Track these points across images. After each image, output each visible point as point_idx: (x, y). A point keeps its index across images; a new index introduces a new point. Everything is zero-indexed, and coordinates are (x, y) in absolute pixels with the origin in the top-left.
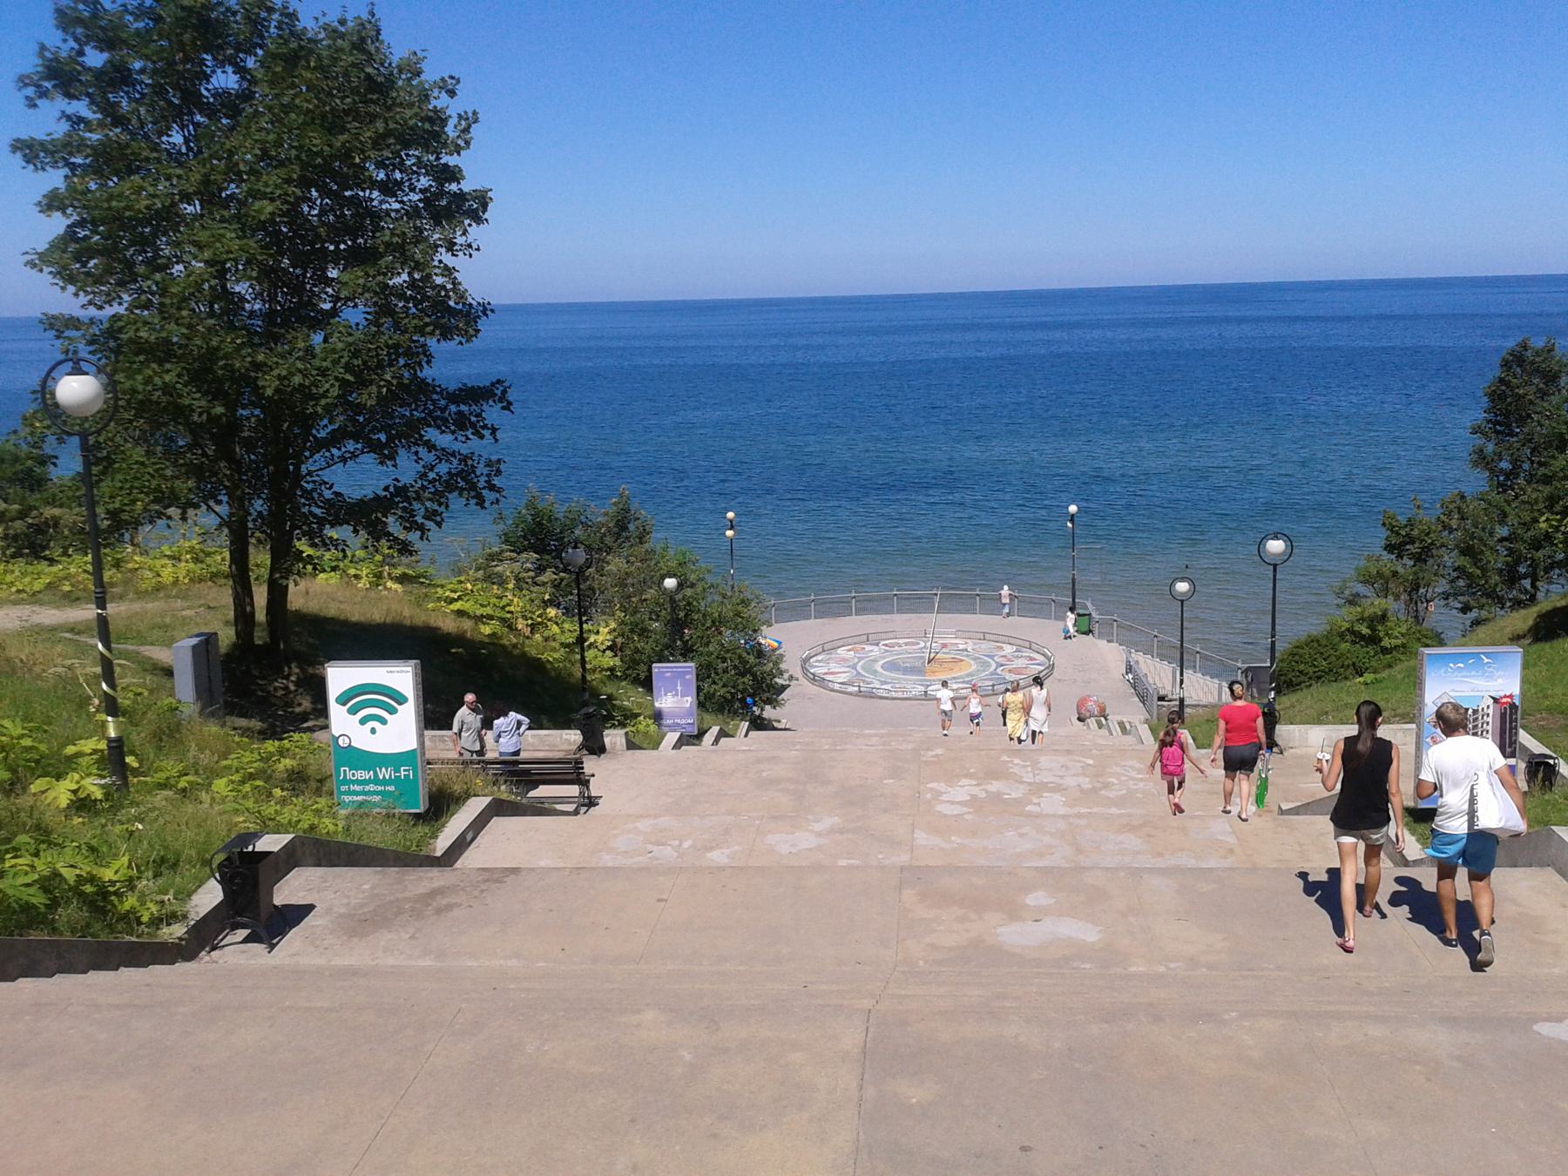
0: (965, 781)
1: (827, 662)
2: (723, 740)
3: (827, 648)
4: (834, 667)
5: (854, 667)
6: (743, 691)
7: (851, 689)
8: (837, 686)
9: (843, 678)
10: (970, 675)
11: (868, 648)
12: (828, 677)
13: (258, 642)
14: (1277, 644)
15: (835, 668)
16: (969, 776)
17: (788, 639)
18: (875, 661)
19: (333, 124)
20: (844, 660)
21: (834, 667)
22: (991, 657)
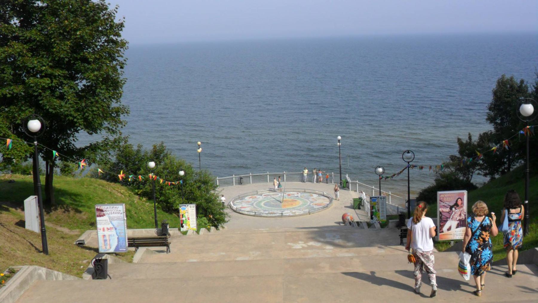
0: (300, 242)
1: (241, 203)
2: (455, 202)
3: (241, 198)
4: (244, 205)
5: (252, 204)
6: (211, 215)
7: (252, 214)
8: (246, 213)
9: (248, 209)
10: (300, 206)
11: (258, 197)
12: (242, 209)
13: (50, 92)
14: (37, 247)
15: (245, 206)
16: (301, 240)
17: (225, 195)
18: (261, 202)
19: (19, 55)
20: (249, 202)
21: (244, 205)
22: (308, 199)
